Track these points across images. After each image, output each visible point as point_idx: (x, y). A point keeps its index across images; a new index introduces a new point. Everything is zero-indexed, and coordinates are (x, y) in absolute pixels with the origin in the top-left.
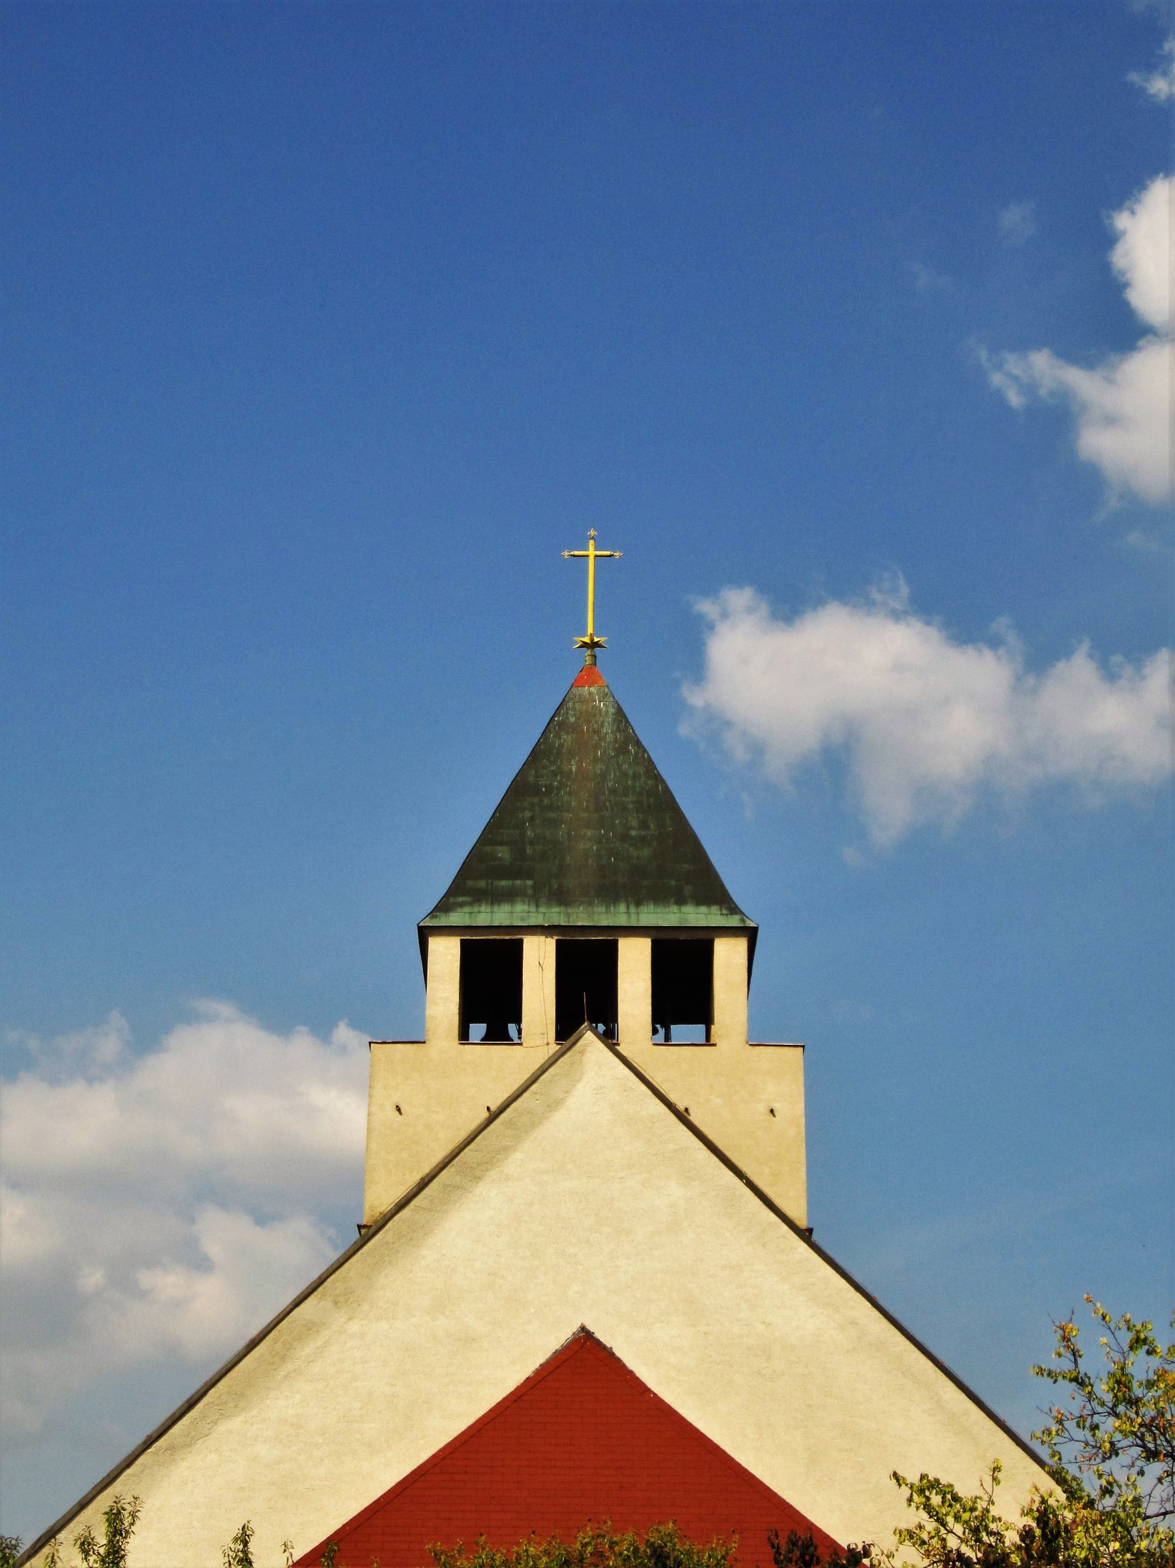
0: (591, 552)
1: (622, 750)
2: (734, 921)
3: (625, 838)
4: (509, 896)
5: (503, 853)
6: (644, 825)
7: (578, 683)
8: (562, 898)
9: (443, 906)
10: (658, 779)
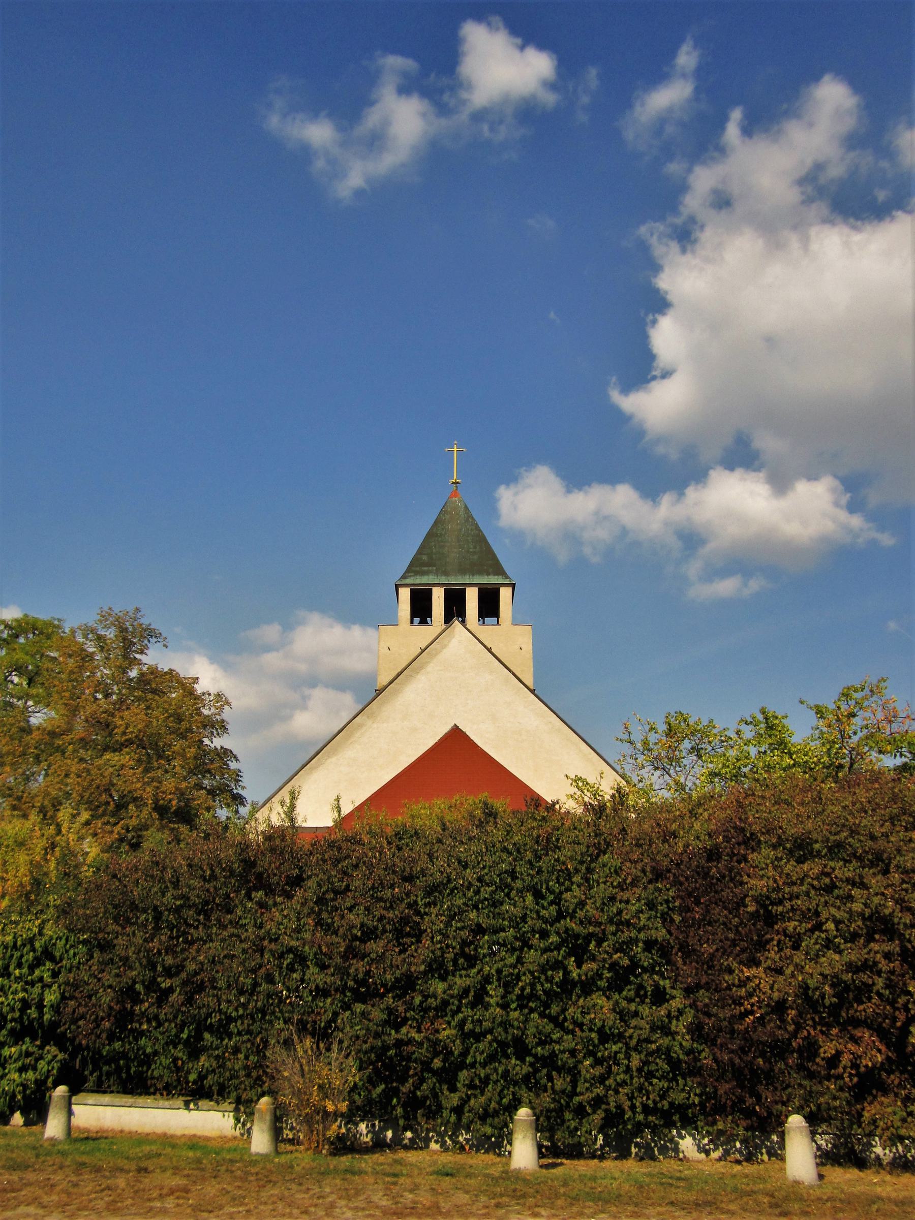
0: (455, 449)
1: (467, 520)
2: (507, 581)
3: (468, 552)
4: (423, 573)
5: (425, 558)
6: (475, 547)
7: (451, 497)
8: (446, 573)
9: (404, 577)
10: (480, 530)
